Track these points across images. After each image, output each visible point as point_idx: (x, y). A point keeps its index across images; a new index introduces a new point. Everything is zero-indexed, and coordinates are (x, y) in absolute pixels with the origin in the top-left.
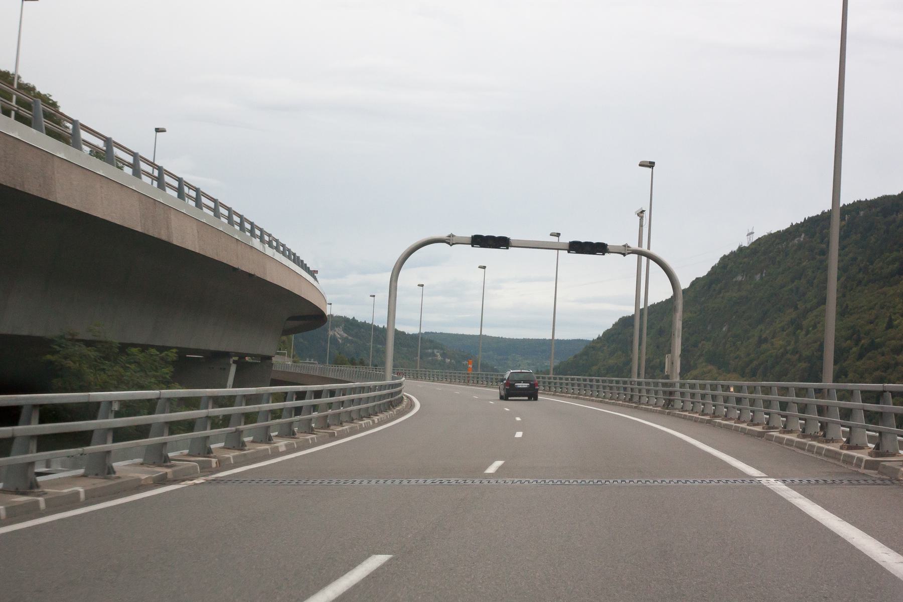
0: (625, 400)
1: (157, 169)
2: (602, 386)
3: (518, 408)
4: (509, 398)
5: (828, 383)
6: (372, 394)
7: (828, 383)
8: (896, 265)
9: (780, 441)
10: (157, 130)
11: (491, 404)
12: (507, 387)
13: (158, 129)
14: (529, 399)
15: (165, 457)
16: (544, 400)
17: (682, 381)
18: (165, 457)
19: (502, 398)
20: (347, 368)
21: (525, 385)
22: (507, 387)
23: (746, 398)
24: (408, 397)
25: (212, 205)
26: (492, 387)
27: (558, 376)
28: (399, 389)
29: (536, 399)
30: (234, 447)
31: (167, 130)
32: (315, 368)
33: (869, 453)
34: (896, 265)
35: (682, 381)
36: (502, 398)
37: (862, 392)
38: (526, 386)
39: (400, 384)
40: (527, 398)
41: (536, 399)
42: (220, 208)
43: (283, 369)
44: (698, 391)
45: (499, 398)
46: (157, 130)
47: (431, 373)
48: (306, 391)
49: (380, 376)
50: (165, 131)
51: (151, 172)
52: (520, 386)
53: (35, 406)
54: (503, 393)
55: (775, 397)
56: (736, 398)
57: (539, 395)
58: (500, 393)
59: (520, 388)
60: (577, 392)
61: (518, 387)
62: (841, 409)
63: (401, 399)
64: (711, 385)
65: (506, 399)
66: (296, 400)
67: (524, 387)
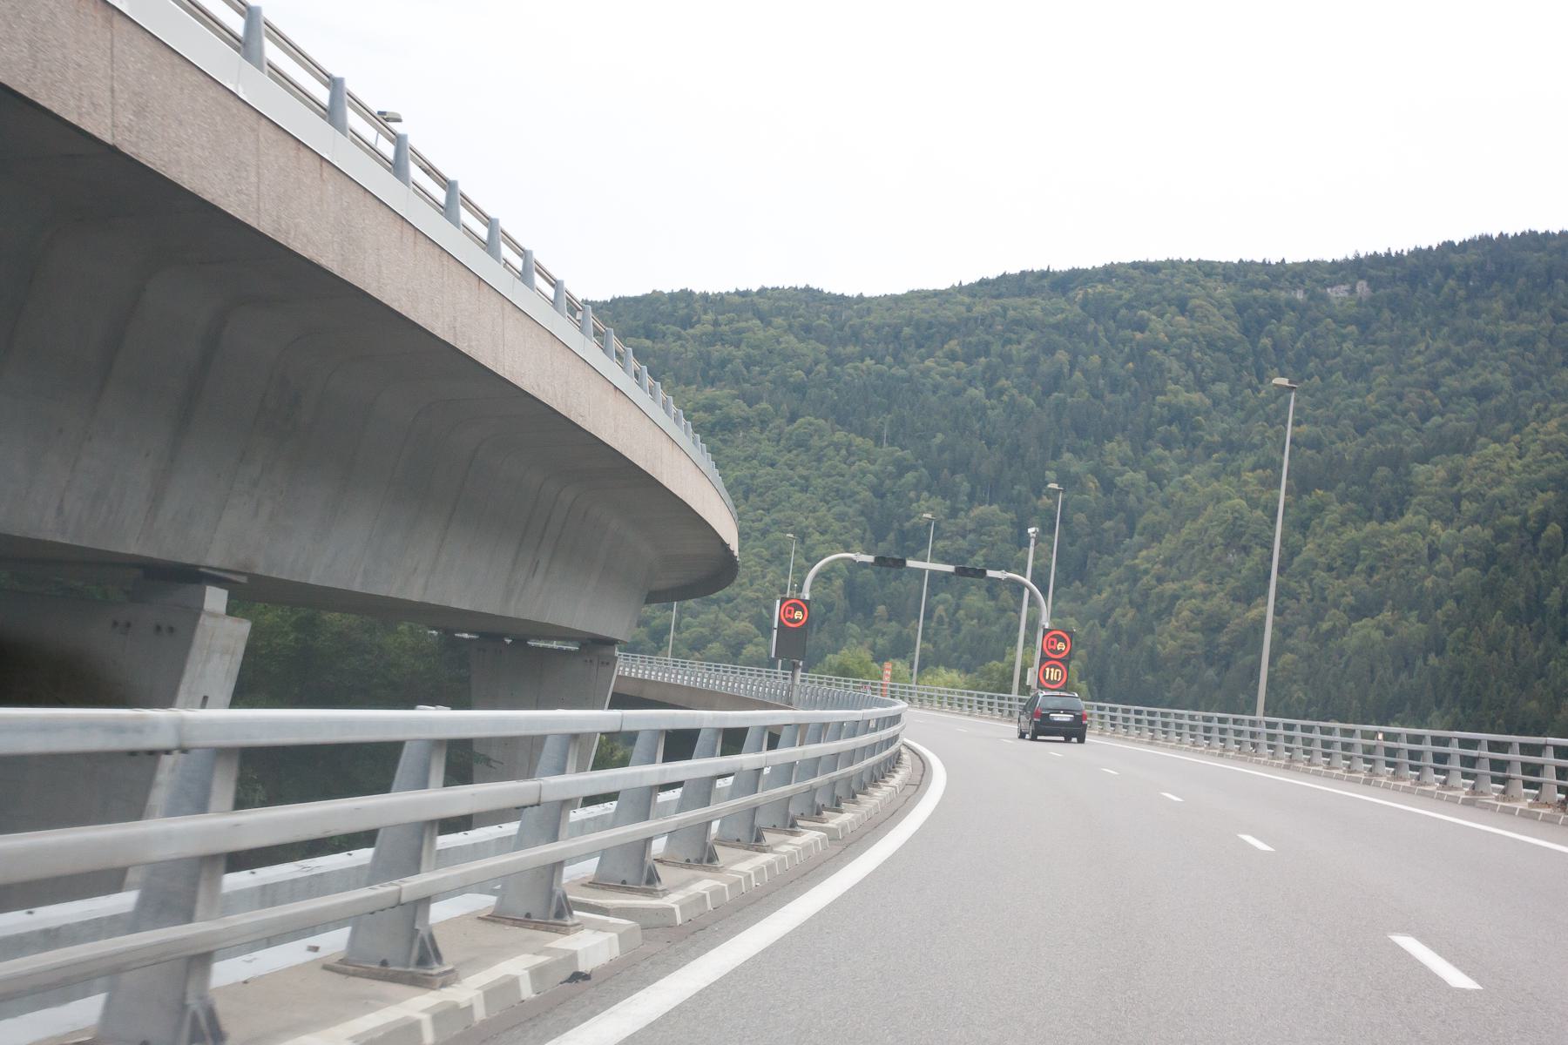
0: (1276, 311)
2: (1174, 724)
3: (1054, 751)
4: (1039, 738)
7: (1259, 717)
8: (1396, 526)
12: (1035, 720)
14: (1068, 740)
15: (423, 941)
16: (1093, 743)
18: (423, 941)
21: (1067, 718)
22: (1035, 720)
25: (518, 263)
29: (1081, 740)
32: (866, 698)
33: (834, 604)
34: (1396, 526)
36: (1022, 736)
38: (1068, 720)
39: (895, 719)
40: (1062, 738)
41: (1081, 740)
42: (462, 208)
43: (685, 682)
47: (985, 700)
48: (748, 728)
49: (848, 697)
51: (371, 140)
52: (1058, 719)
56: (1461, 756)
57: (1087, 736)
59: (1057, 722)
61: (1055, 719)
62: (1322, 741)
63: (897, 758)
65: (1034, 739)
66: (665, 760)
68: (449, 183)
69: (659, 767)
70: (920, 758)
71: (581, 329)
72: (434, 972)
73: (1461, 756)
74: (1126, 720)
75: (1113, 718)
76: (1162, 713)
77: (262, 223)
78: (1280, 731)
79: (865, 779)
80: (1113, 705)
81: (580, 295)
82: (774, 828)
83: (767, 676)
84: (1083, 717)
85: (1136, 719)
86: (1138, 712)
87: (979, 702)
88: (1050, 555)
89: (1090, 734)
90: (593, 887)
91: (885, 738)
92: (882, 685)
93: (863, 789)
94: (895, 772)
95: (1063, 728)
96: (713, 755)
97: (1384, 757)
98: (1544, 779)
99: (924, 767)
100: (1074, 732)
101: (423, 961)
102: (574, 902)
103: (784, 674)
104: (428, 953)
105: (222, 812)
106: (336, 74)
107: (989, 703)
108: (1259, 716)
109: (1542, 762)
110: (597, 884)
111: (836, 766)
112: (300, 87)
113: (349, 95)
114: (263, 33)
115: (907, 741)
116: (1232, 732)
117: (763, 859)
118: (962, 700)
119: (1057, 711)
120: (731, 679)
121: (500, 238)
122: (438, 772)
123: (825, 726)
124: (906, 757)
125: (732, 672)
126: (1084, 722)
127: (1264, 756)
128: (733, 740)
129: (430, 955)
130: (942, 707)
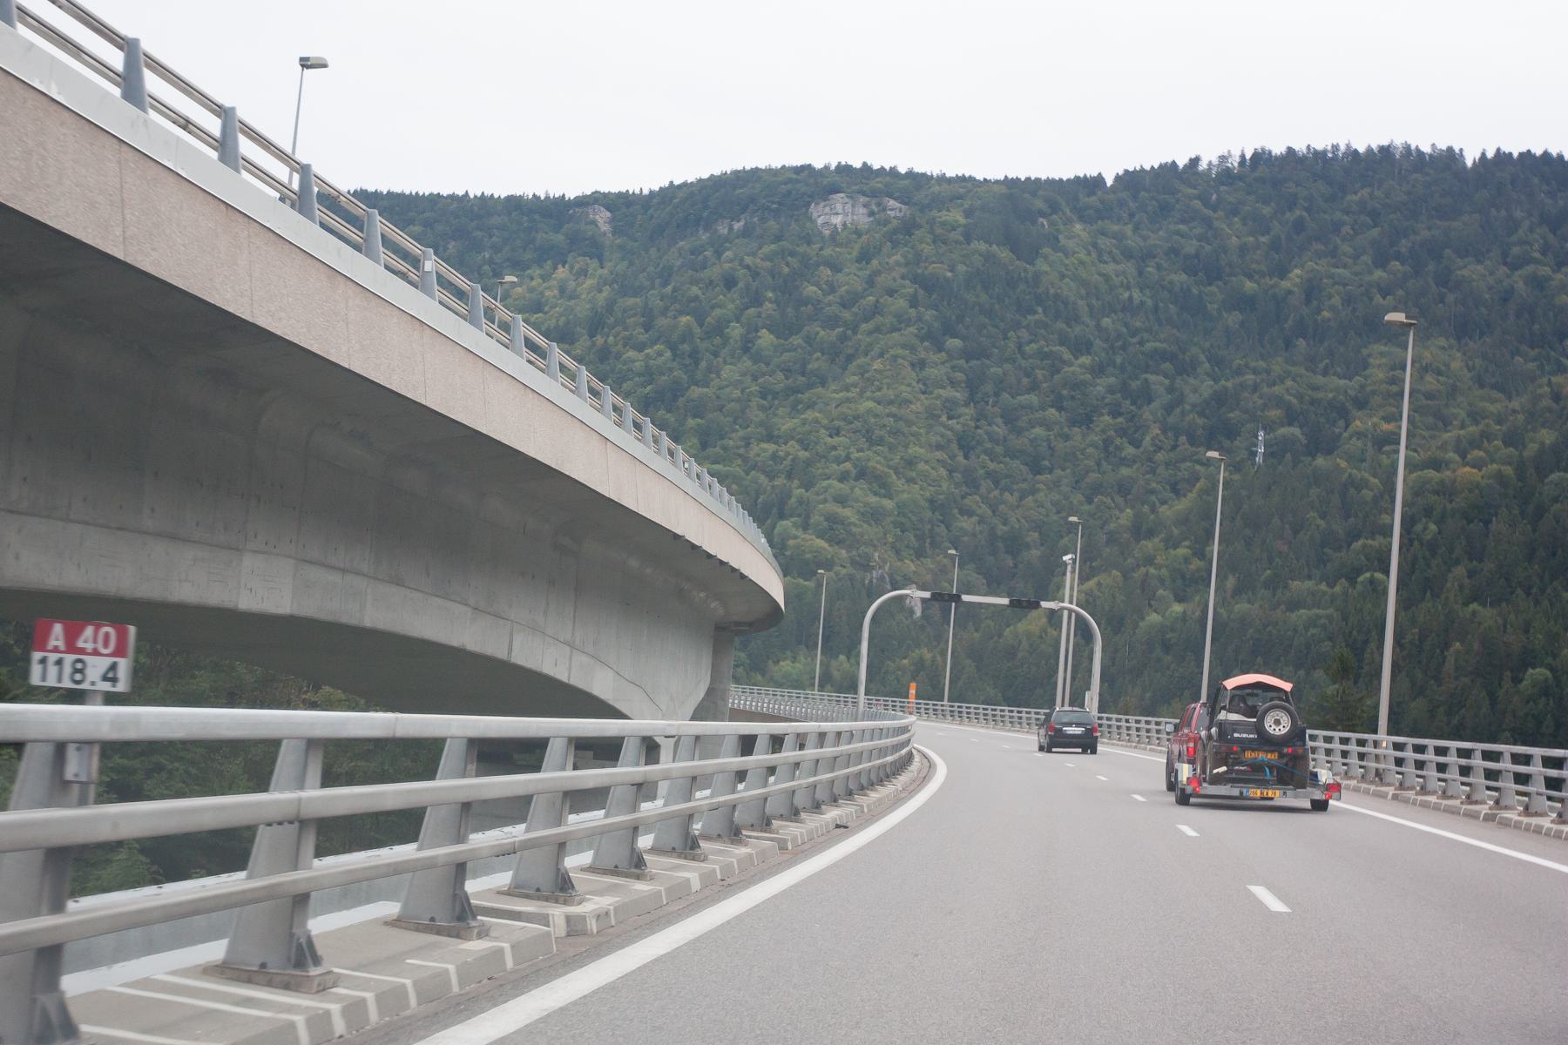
1: (298, 172)
3: (1070, 762)
4: (1054, 750)
5: (945, 703)
6: (857, 746)
7: (945, 703)
9: (1517, 826)
10: (306, 63)
11: (1102, 775)
13: (307, 59)
14: (1084, 752)
15: (300, 946)
17: (1100, 715)
19: (1041, 749)
20: (756, 845)
23: (1432, 762)
24: (925, 756)
26: (1014, 731)
27: (1104, 715)
28: (906, 736)
29: (1094, 752)
30: (674, 849)
31: (329, 64)
35: (1100, 715)
36: (1041, 749)
37: (1413, 745)
38: (1080, 733)
40: (1080, 750)
41: (1094, 752)
44: (1123, 724)
45: (1037, 749)
46: (306, 63)
48: (757, 736)
50: (325, 66)
51: (285, 180)
52: (1071, 732)
53: (312, 743)
54: (1044, 741)
55: (1336, 746)
56: (1325, 749)
58: (1040, 742)
60: (1434, 784)
62: (1396, 758)
63: (910, 756)
64: (1341, 739)
65: (1049, 751)
67: (1077, 733)
68: (225, 111)
69: (570, 773)
70: (929, 761)
71: (689, 475)
72: (311, 974)
73: (1325, 749)
74: (1119, 727)
75: (985, 715)
76: (1341, 739)
77: (428, 398)
78: (1506, 765)
79: (864, 781)
80: (1138, 718)
81: (345, 178)
82: (781, 817)
83: (853, 702)
84: (1093, 730)
85: (1416, 762)
86: (1465, 754)
87: (951, 711)
88: (1052, 632)
89: (1103, 743)
90: (397, 927)
91: (896, 743)
92: (908, 703)
93: (862, 789)
94: (900, 775)
95: (1074, 741)
96: (795, 750)
97: (1414, 771)
98: (1407, 770)
99: (931, 766)
100: (1087, 744)
101: (300, 963)
102: (478, 907)
103: (820, 695)
104: (303, 955)
105: (313, 788)
106: (227, 104)
107: (926, 709)
108: (1382, 736)
109: (1446, 762)
110: (515, 891)
111: (861, 761)
112: (107, 65)
113: (241, 123)
114: (142, 63)
115: (915, 745)
116: (1007, 717)
117: (742, 851)
118: (978, 714)
119: (1070, 724)
120: (749, 699)
121: (238, 129)
122: (315, 772)
123: (839, 734)
124: (917, 758)
125: (773, 695)
126: (1095, 734)
127: (1483, 802)
128: (777, 742)
129: (306, 958)
130: (953, 720)
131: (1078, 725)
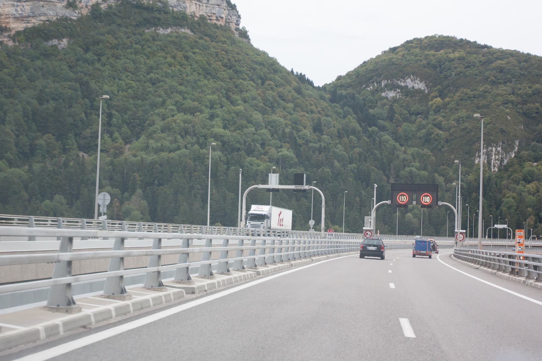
21: (374, 248)
38: (375, 249)
52: (370, 249)
119: (370, 245)
131: (374, 246)
